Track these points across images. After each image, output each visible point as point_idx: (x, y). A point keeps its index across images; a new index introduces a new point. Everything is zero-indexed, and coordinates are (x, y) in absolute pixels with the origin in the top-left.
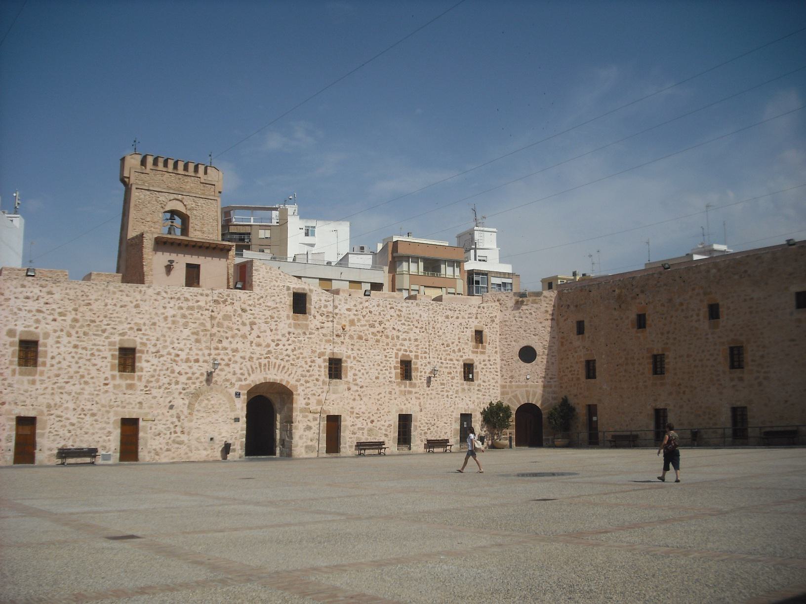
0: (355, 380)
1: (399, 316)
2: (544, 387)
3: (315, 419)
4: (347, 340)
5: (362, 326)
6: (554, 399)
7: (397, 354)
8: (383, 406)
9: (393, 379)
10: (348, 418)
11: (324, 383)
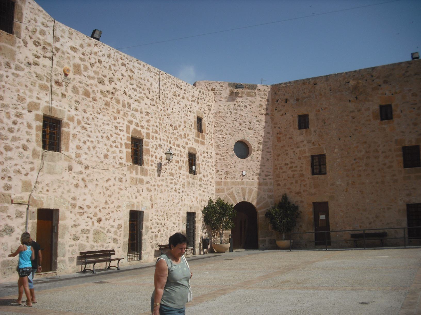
0: (78, 156)
1: (131, 77)
2: (260, 184)
3: (19, 215)
4: (69, 93)
5: (89, 77)
6: (270, 197)
7: (128, 127)
8: (112, 199)
9: (124, 161)
10: (68, 214)
11: (35, 154)
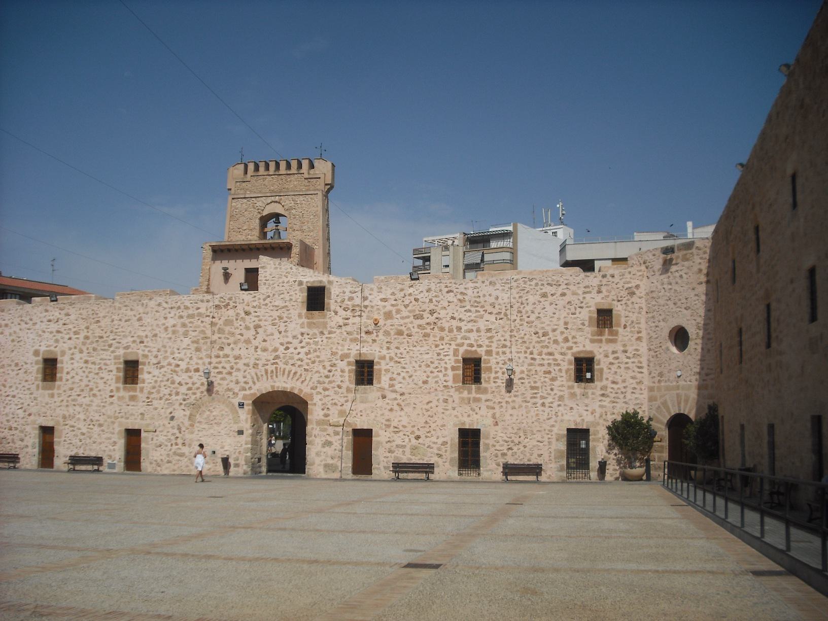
0: (392, 386)
2: (700, 388)
3: (336, 433)
8: (435, 418)
10: (382, 432)
